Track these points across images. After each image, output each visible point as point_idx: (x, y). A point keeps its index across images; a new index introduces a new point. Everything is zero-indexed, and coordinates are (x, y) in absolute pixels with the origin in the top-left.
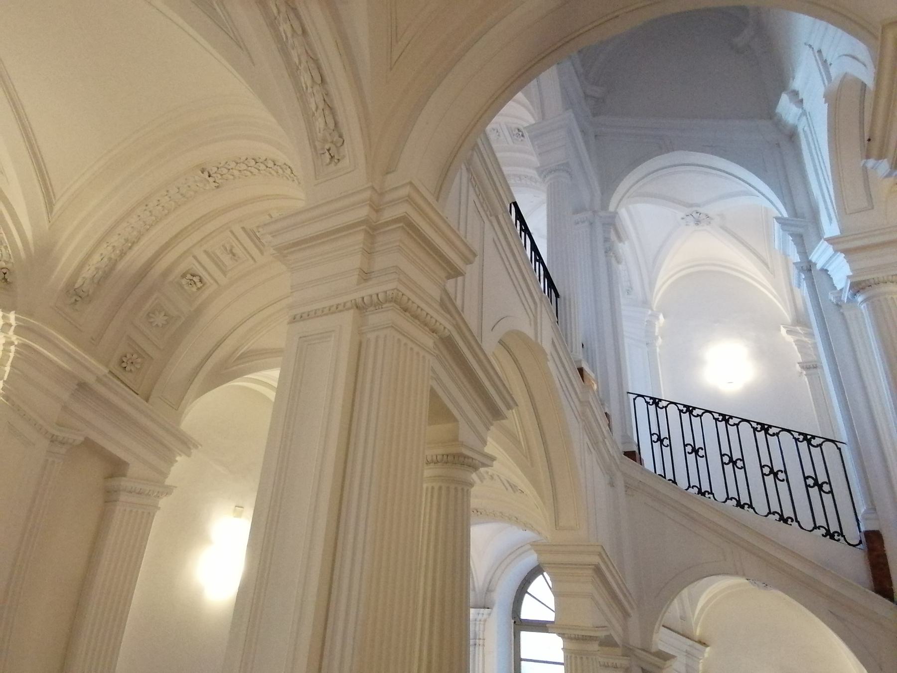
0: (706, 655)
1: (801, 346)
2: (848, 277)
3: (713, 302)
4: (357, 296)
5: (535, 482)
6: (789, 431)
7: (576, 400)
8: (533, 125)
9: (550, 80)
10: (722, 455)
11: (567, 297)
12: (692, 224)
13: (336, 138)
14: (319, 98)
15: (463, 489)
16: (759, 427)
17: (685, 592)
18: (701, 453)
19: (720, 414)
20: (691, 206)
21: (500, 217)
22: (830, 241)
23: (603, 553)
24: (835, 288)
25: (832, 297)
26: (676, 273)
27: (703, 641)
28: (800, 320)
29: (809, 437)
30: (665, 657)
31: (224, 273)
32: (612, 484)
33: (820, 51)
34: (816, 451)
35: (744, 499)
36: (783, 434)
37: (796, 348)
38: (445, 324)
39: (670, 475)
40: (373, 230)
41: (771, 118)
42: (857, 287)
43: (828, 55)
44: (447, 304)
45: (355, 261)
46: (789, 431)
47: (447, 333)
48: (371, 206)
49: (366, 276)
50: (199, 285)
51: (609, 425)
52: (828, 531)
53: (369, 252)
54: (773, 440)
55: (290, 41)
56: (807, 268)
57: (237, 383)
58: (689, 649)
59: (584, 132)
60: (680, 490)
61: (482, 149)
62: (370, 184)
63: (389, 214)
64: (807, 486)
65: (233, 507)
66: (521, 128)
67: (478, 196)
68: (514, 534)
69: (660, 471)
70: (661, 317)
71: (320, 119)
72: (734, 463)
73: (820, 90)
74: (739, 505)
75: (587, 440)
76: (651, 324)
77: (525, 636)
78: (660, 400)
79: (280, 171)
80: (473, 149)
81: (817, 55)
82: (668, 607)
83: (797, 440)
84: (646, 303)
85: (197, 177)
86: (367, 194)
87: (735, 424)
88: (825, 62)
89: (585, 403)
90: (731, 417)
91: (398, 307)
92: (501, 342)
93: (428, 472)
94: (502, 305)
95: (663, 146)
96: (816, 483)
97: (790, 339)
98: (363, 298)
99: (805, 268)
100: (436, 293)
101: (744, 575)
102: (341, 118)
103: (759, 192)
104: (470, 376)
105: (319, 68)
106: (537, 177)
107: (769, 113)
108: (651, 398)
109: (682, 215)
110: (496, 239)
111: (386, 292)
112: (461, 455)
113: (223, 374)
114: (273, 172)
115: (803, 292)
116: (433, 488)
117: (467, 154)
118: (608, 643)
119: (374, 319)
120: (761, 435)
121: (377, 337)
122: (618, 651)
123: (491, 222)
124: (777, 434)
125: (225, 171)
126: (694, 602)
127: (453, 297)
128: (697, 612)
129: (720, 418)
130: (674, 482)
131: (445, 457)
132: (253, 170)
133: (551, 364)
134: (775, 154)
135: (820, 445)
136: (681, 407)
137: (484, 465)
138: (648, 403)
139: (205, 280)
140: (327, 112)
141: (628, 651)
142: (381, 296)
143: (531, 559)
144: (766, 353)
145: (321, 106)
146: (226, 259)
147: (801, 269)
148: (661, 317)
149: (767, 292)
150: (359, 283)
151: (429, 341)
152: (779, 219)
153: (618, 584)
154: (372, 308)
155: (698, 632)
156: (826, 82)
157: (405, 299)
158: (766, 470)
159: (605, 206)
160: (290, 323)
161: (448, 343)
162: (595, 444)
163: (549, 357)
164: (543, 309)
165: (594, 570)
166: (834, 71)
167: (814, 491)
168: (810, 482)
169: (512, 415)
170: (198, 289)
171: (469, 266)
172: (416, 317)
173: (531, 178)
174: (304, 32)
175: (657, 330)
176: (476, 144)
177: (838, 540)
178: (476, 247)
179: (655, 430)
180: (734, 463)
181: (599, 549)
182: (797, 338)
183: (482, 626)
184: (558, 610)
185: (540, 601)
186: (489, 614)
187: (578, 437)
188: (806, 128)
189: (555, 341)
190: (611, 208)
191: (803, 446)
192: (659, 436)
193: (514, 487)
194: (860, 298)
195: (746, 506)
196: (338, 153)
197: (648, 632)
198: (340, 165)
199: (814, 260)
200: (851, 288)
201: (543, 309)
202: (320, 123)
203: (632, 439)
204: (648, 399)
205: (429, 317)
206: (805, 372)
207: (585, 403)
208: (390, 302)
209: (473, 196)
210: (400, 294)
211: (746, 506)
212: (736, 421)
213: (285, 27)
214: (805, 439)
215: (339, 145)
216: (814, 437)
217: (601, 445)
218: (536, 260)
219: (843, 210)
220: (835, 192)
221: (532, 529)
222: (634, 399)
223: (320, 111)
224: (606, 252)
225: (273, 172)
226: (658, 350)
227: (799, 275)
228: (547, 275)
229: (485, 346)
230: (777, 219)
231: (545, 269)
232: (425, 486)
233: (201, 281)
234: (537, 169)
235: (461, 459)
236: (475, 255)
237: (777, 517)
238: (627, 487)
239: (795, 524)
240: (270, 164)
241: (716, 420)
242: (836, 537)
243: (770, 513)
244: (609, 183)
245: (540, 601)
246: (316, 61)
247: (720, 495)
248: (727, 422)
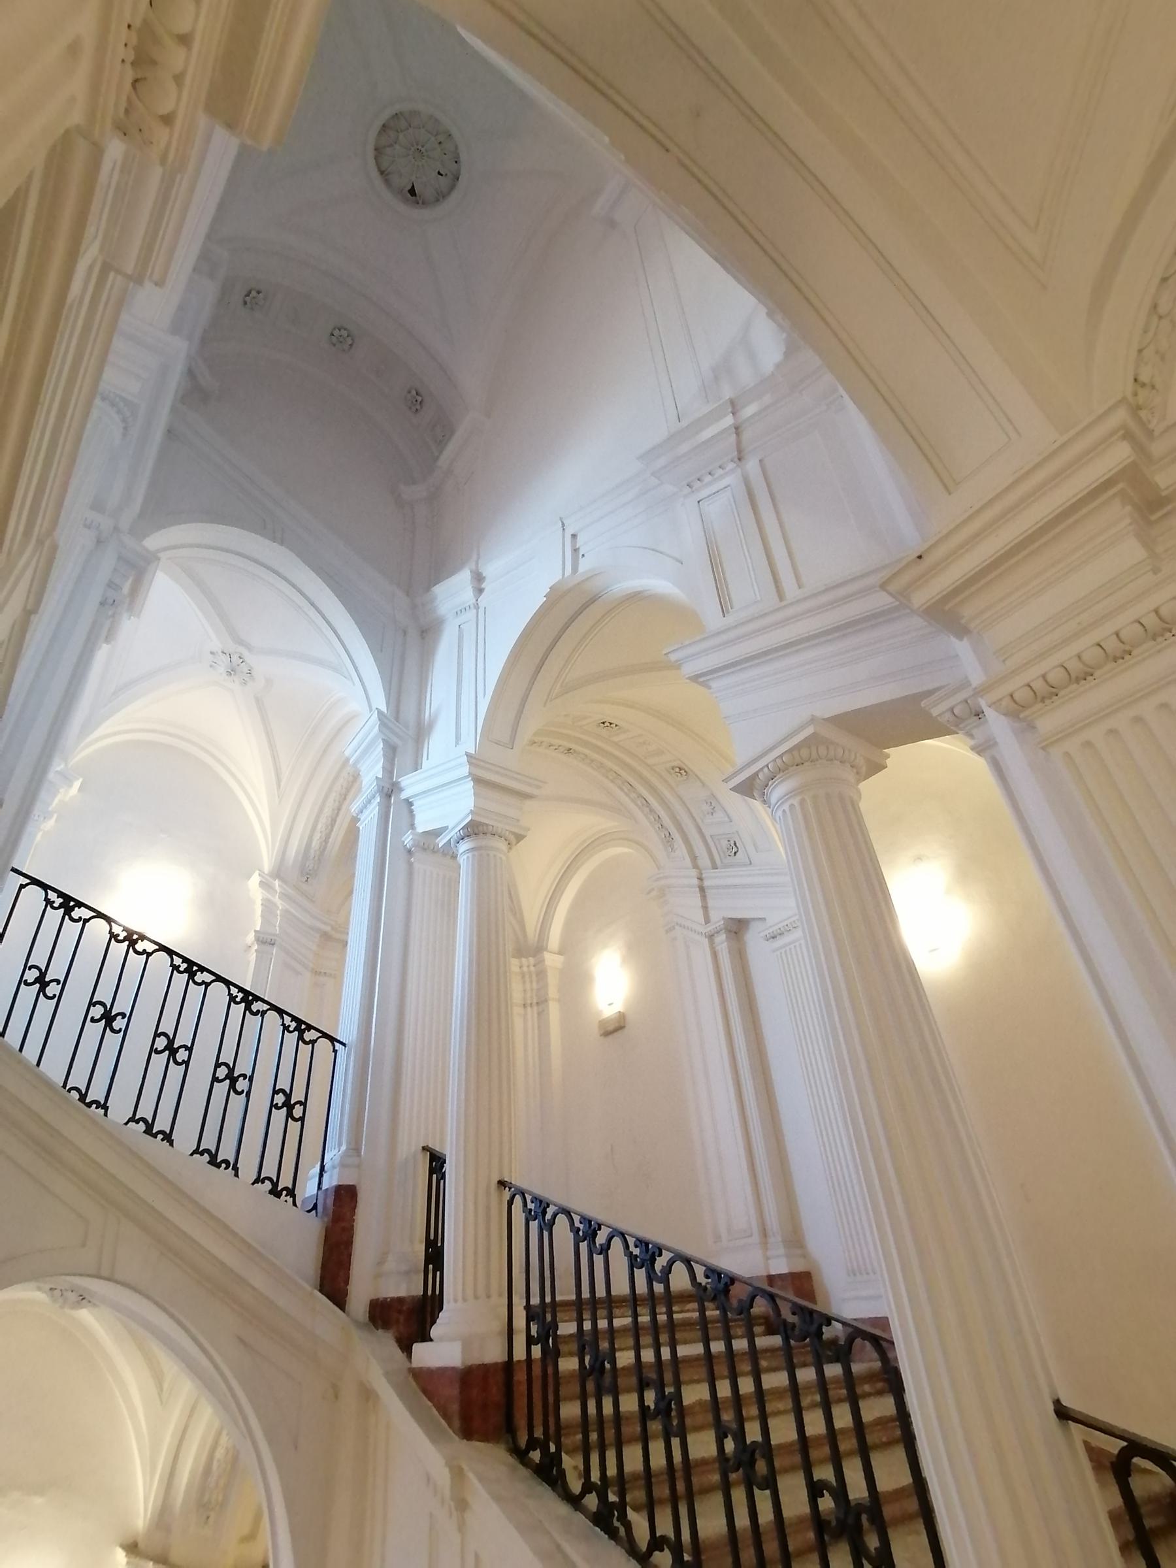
1: (268, 906)
3: (172, 796)
12: (222, 670)
20: (240, 642)
36: (272, 1015)
37: (259, 909)
70: (77, 784)
88: (576, 550)
109: (216, 645)
134: (406, 640)
135: (313, 1042)
148: (77, 784)
152: (380, 712)
166: (584, 566)
175: (56, 801)
190: (153, 542)
199: (403, 784)
201: (29, 573)
204: (52, 896)
206: (256, 947)
212: (208, 977)
224: (102, 604)
244: (161, 509)
247: (120, 1108)
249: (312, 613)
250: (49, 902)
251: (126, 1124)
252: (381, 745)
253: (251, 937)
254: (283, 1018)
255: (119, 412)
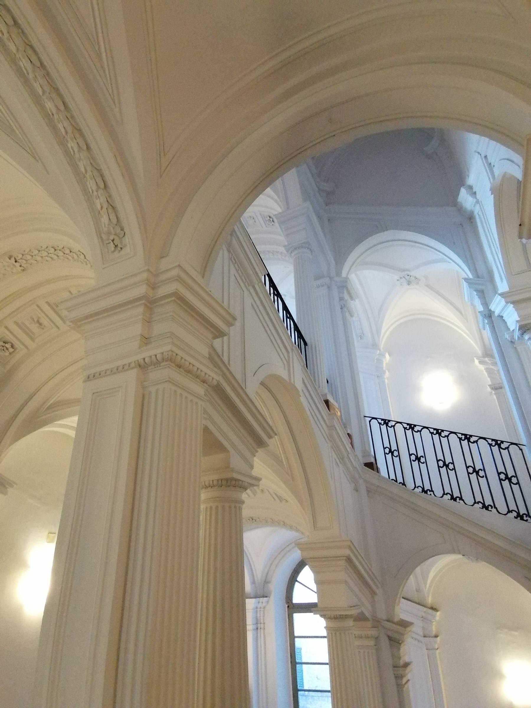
0: (437, 618)
1: (490, 372)
2: (517, 321)
3: (423, 343)
4: (139, 357)
5: (295, 493)
6: (484, 439)
7: (324, 426)
8: (280, 213)
9: (291, 179)
10: (438, 461)
11: (313, 346)
12: (405, 284)
13: (118, 230)
14: (103, 199)
15: (235, 507)
16: (463, 437)
17: (418, 570)
18: (422, 460)
19: (434, 429)
20: (404, 270)
21: (256, 286)
22: (501, 295)
23: (352, 547)
24: (509, 329)
25: (507, 336)
26: (398, 320)
27: (435, 607)
28: (487, 354)
29: (499, 442)
30: (405, 624)
31: (33, 340)
32: (356, 490)
33: (486, 157)
34: (505, 453)
35: (456, 494)
36: (481, 442)
37: (486, 374)
38: (214, 376)
39: (400, 480)
40: (150, 304)
41: (455, 206)
42: (524, 329)
43: (491, 159)
44: (215, 359)
45: (137, 329)
46: (484, 439)
47: (215, 383)
48: (147, 284)
49: (146, 340)
50: (11, 350)
51: (352, 444)
52: (518, 513)
53: (148, 322)
54: (473, 446)
55: (77, 155)
56: (489, 315)
57: (48, 429)
58: (424, 615)
59: (319, 217)
60: (408, 490)
61: (238, 234)
62: (146, 268)
63: (163, 291)
64: (501, 480)
65: (46, 533)
66: (272, 216)
67: (237, 271)
68: (284, 535)
69: (392, 477)
70: (387, 355)
71: (105, 217)
72: (447, 466)
73: (488, 186)
74: (453, 498)
75: (334, 456)
76: (379, 361)
77: (297, 616)
78: (389, 421)
79: (75, 256)
80: (231, 235)
81: (484, 160)
82: (405, 584)
83: (490, 445)
84: (375, 345)
85: (5, 263)
86: (145, 275)
87: (445, 436)
89: (331, 427)
90: (443, 431)
91: (173, 365)
92: (262, 384)
93: (203, 496)
94: (261, 354)
95: (378, 227)
96: (507, 477)
97: (482, 367)
98: (144, 359)
99: (487, 315)
100: (205, 351)
101: (460, 553)
102: (122, 215)
103: (451, 259)
104: (236, 416)
105: (102, 176)
106: (286, 252)
107: (454, 202)
108: (382, 420)
109: (396, 277)
110: (254, 304)
111: (162, 353)
112: (232, 479)
113: (34, 422)
114: (70, 258)
115: (487, 333)
116: (211, 508)
117: (228, 239)
118: (360, 618)
119: (154, 375)
120: (465, 443)
121: (157, 391)
122: (369, 624)
123: (249, 290)
124: (476, 442)
125: (29, 257)
126: (425, 576)
127: (220, 353)
128: (428, 585)
129: (435, 432)
130: (404, 484)
131: (220, 482)
132: (53, 256)
133: (303, 399)
134: (460, 232)
135: (507, 448)
136: (405, 426)
137: (253, 485)
138: (380, 424)
139: (16, 346)
140: (110, 211)
141: (377, 623)
142: (159, 357)
143: (296, 555)
144: (465, 379)
145: (105, 205)
146: (34, 328)
147: (485, 316)
148: (387, 355)
149: (462, 333)
150: (140, 348)
151: (200, 390)
152: (466, 280)
153: (365, 570)
154: (153, 367)
155: (430, 600)
156: (492, 180)
157: (179, 358)
158: (471, 470)
159: (339, 274)
160: (85, 381)
161: (218, 389)
162: (342, 459)
163: (301, 393)
164: (295, 356)
165: (346, 560)
166: (497, 172)
167: (506, 483)
168: (503, 476)
169: (273, 443)
170: (10, 354)
171: (232, 328)
172: (188, 372)
173: (281, 253)
174: (88, 148)
176: (234, 231)
177: (527, 521)
178: (238, 314)
179: (387, 444)
180: (447, 466)
181: (349, 543)
182: (486, 367)
183: (262, 612)
184: (320, 593)
185: (306, 591)
186: (268, 602)
187: (328, 455)
188: (480, 213)
189: (305, 379)
190: (344, 274)
191: (495, 449)
192: (390, 449)
193: (280, 499)
194: (526, 337)
195: (458, 499)
196: (121, 243)
197: (391, 605)
198: (123, 252)
199: (492, 309)
200: (519, 330)
202: (105, 219)
203: (370, 453)
204: (380, 421)
205: (199, 371)
207: (331, 427)
208: (167, 361)
209: (233, 271)
210: (175, 354)
211: (458, 499)
212: (446, 433)
213: (72, 144)
214: (497, 444)
215: (121, 236)
216: (502, 442)
217: (346, 460)
218: (287, 317)
219: (510, 274)
220: (503, 260)
221: (297, 530)
222: (370, 421)
223: (104, 209)
224: (341, 308)
225: (70, 258)
226: (386, 381)
227: (484, 321)
228: (296, 328)
229: (248, 391)
230: (465, 279)
231: (295, 324)
232: (203, 507)
233: (12, 346)
234: (285, 246)
235: (233, 482)
236: (235, 319)
237: (480, 505)
238: (368, 491)
239: (494, 510)
240: (67, 251)
241: (432, 433)
242: (525, 518)
243: (475, 503)
244: (340, 257)
245: (306, 591)
246: (99, 171)
247: (439, 492)
248: (440, 434)
249: (417, 245)
250: (380, 424)
251: (442, 497)
252: (475, 293)
253: (489, 389)
254: (487, 441)
255: (305, 248)
